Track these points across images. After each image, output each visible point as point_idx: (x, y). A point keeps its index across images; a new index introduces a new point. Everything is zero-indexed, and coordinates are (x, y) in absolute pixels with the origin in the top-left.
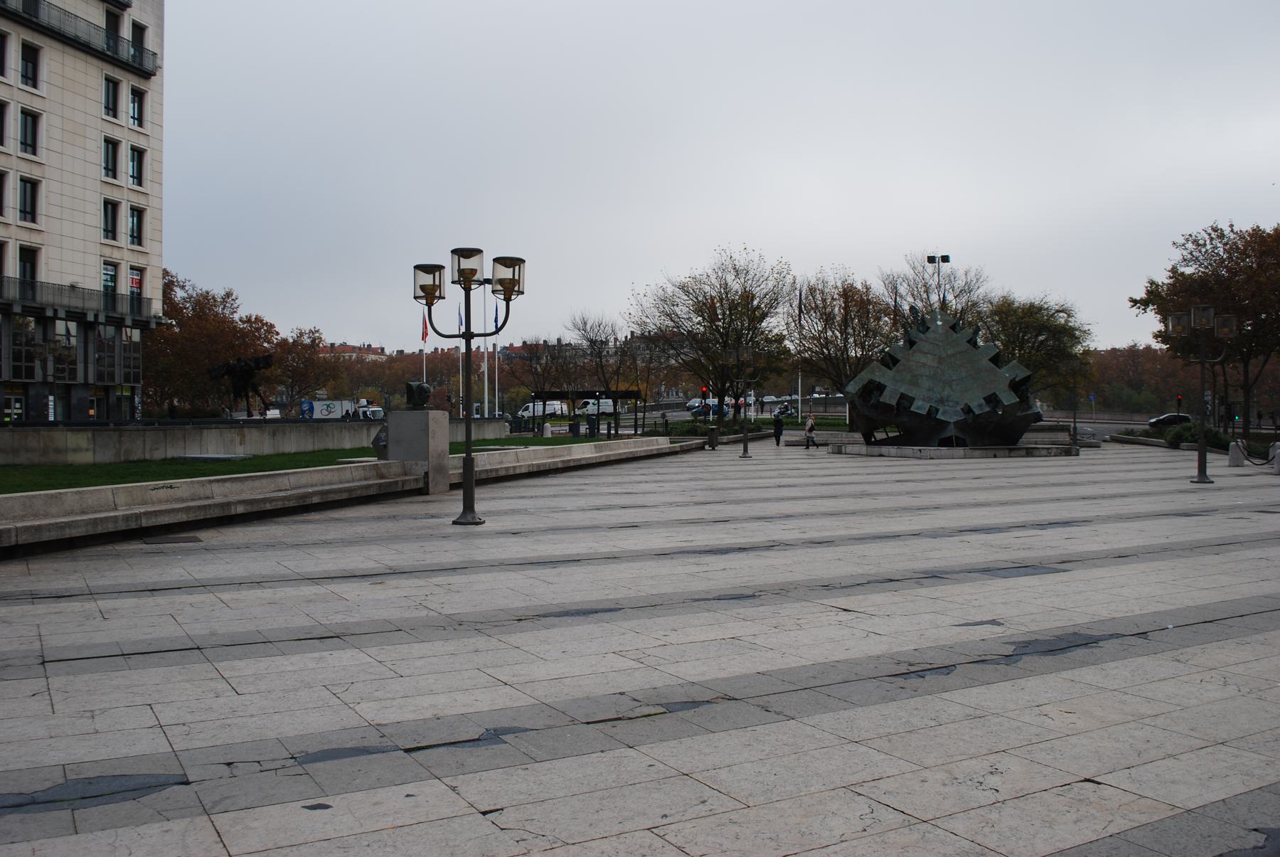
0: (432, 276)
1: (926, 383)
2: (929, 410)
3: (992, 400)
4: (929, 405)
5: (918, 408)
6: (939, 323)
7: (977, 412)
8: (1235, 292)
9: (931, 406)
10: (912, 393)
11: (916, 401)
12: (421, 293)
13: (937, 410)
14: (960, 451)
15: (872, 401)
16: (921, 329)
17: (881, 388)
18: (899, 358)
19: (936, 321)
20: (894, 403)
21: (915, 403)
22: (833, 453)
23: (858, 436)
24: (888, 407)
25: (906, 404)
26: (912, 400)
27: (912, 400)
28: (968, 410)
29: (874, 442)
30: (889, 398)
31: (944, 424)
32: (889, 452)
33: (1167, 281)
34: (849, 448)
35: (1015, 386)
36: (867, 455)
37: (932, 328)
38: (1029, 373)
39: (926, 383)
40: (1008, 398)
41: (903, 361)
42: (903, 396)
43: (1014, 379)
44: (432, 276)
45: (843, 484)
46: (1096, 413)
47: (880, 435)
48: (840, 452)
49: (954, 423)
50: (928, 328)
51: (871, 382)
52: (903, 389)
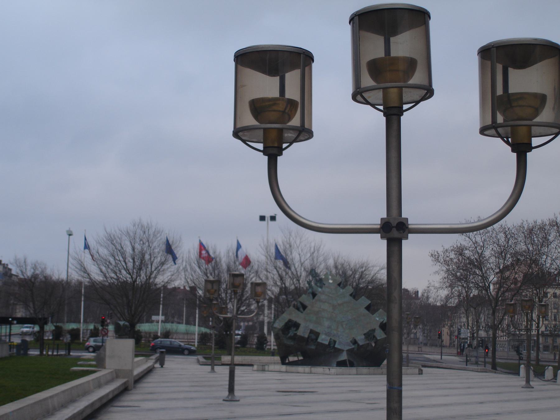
0: (277, 79)
1: (327, 323)
2: (330, 342)
3: (370, 335)
4: (329, 338)
5: (323, 340)
6: (331, 281)
7: (361, 343)
8: (527, 267)
9: (331, 339)
10: (318, 330)
11: (321, 335)
12: (249, 120)
13: (335, 342)
14: (353, 370)
15: (289, 335)
16: (318, 284)
17: (297, 326)
18: (307, 305)
19: (328, 280)
20: (306, 336)
21: (320, 337)
22: (257, 370)
23: (277, 358)
24: (302, 338)
25: (313, 337)
27: (317, 334)
28: (355, 342)
29: (288, 363)
30: (302, 332)
31: (340, 351)
32: (304, 370)
33: (86, 283)
34: (272, 367)
35: (383, 326)
36: (286, 372)
37: (327, 285)
39: (327, 323)
40: (380, 335)
41: (309, 307)
42: (312, 332)
43: (383, 322)
44: (277, 79)
45: (336, 412)
46: (199, 326)
47: (292, 359)
48: (263, 370)
49: (348, 351)
51: (290, 321)
52: (311, 326)
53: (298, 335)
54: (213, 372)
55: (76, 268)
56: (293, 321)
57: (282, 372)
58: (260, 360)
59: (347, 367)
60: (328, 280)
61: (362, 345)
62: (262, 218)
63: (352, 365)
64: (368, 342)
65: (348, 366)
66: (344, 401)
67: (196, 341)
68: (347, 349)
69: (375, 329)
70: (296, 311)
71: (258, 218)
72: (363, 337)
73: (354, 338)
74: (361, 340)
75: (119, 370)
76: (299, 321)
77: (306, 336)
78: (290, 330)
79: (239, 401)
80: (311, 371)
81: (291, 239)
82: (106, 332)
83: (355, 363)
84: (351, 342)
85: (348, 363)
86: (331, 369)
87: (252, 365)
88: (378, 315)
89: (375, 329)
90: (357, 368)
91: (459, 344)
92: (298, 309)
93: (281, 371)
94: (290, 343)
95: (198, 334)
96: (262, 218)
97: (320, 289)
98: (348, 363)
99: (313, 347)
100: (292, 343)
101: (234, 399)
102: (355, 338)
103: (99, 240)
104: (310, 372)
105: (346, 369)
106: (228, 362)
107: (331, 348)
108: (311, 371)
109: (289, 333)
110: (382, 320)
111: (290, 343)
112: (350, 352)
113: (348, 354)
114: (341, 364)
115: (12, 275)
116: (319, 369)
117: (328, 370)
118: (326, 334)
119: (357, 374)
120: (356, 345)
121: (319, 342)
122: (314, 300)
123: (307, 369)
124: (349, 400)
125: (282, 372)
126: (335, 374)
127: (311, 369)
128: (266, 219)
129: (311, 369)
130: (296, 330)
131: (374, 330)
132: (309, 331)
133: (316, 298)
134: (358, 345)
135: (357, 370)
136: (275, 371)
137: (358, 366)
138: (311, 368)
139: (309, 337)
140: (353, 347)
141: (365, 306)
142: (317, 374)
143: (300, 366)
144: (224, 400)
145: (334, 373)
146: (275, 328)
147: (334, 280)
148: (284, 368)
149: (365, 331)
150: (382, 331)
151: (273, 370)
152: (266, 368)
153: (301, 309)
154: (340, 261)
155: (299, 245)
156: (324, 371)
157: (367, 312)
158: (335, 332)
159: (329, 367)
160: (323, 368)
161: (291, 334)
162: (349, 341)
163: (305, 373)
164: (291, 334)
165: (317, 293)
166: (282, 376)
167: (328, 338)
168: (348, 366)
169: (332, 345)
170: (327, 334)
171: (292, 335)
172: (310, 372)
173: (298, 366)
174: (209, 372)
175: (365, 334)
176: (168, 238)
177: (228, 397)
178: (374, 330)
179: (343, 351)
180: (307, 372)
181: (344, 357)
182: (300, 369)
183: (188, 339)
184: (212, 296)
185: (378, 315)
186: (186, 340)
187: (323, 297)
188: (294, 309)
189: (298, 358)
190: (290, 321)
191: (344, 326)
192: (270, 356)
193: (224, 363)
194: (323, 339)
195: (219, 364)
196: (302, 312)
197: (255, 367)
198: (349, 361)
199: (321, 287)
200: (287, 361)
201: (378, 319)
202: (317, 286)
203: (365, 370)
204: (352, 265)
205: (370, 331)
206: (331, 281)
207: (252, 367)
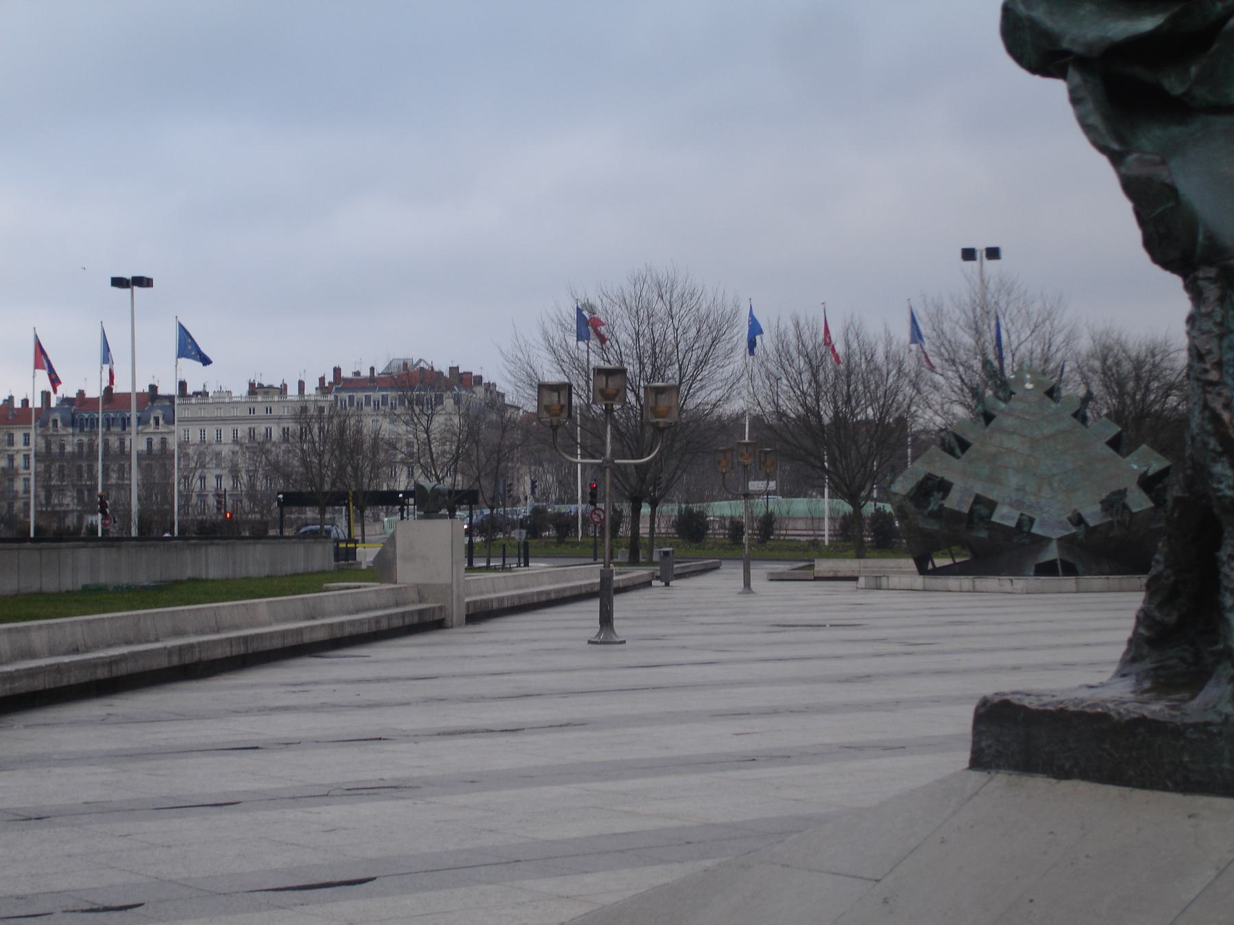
1: (1014, 480)
3: (1114, 503)
4: (1019, 512)
5: (1003, 517)
6: (1029, 386)
9: (1022, 515)
13: (1032, 521)
14: (1070, 582)
15: (930, 508)
17: (944, 487)
19: (1024, 383)
24: (955, 516)
25: (984, 511)
26: (992, 505)
27: (992, 505)
28: (1078, 520)
29: (932, 570)
30: (957, 501)
31: (1042, 541)
34: (895, 581)
37: (1019, 393)
38: (1165, 463)
39: (1014, 480)
41: (976, 446)
42: (978, 499)
43: (1146, 472)
47: (940, 562)
49: (1060, 539)
50: (1012, 393)
52: (978, 489)
53: (946, 508)
54: (747, 593)
55: (521, 381)
56: (938, 477)
57: (915, 590)
58: (901, 568)
59: (1058, 576)
60: (1023, 382)
61: (1096, 528)
62: (969, 254)
63: (1070, 570)
64: (1110, 519)
65: (1060, 573)
66: (849, 641)
67: (826, 533)
68: (1060, 536)
69: (1126, 490)
70: (946, 455)
71: (959, 254)
72: (1098, 507)
73: (1075, 511)
74: (1093, 514)
75: (425, 585)
76: (949, 477)
77: (966, 510)
78: (932, 499)
79: (624, 642)
80: (974, 587)
81: (989, 296)
82: (602, 517)
83: (1079, 567)
84: (1070, 519)
85: (1059, 567)
86: (1014, 581)
87: (855, 579)
88: (1136, 458)
89: (1126, 490)
90: (1078, 578)
91: (589, 490)
92: (951, 452)
93: (914, 588)
94: (932, 526)
95: (831, 518)
96: (969, 254)
97: (1003, 405)
98: (1059, 567)
99: (983, 534)
100: (936, 527)
101: (611, 640)
102: (1079, 511)
103: (561, 319)
104: (972, 589)
105: (1054, 579)
106: (829, 572)
107: (1025, 535)
108: (974, 587)
109: (929, 504)
110: (1144, 469)
111: (932, 526)
112: (1067, 543)
113: (1060, 547)
114: (1046, 569)
115: (505, 407)
116: (991, 583)
117: (1010, 582)
118: (1011, 505)
119: (1077, 592)
120: (1082, 526)
121: (993, 523)
122: (987, 430)
123: (966, 582)
124: (886, 639)
125: (915, 590)
126: (1024, 591)
127: (974, 582)
128: (978, 255)
129: (974, 582)
130: (943, 498)
131: (1122, 493)
132: (972, 500)
133: (993, 424)
134: (1086, 525)
135: (1076, 583)
136: (901, 588)
137: (1089, 572)
138: (975, 580)
139: (971, 511)
140: (1074, 530)
141: (1108, 438)
142: (987, 592)
143: (951, 577)
144: (590, 642)
145: (1022, 590)
146: (895, 494)
147: (1037, 383)
148: (919, 581)
149: (1104, 496)
150: (1143, 495)
151: (898, 588)
152: (884, 581)
153: (958, 451)
154: (1123, 338)
155: (1006, 310)
156: (1000, 585)
157: (1111, 451)
158: (1033, 499)
159: (1010, 577)
160: (999, 579)
161: (933, 506)
162: (1064, 518)
163: (962, 592)
164: (933, 506)
165: (995, 413)
166: (887, 598)
167: (1016, 514)
168: (1060, 573)
169: (1026, 529)
170: (1017, 504)
171: (936, 508)
172: (972, 589)
173: (946, 577)
174: (739, 593)
175: (1102, 502)
176: (913, 307)
177: (598, 635)
178: (1122, 493)
179: (1049, 540)
180: (966, 590)
181: (1052, 553)
182: (953, 582)
183: (813, 530)
184: (555, 419)
185: (1136, 458)
186: (811, 533)
187: (1008, 422)
188: (939, 450)
189: (954, 561)
190: (929, 477)
191: (1055, 485)
192: (851, 557)
193: (820, 575)
194: (1005, 516)
195: (809, 578)
196: (958, 458)
197: (862, 581)
198: (1062, 561)
199: (1006, 401)
200: (930, 566)
201: (1135, 467)
202: (998, 398)
203: (1097, 581)
204: (1134, 354)
205: (1114, 494)
206: (1029, 386)
207: (855, 582)
